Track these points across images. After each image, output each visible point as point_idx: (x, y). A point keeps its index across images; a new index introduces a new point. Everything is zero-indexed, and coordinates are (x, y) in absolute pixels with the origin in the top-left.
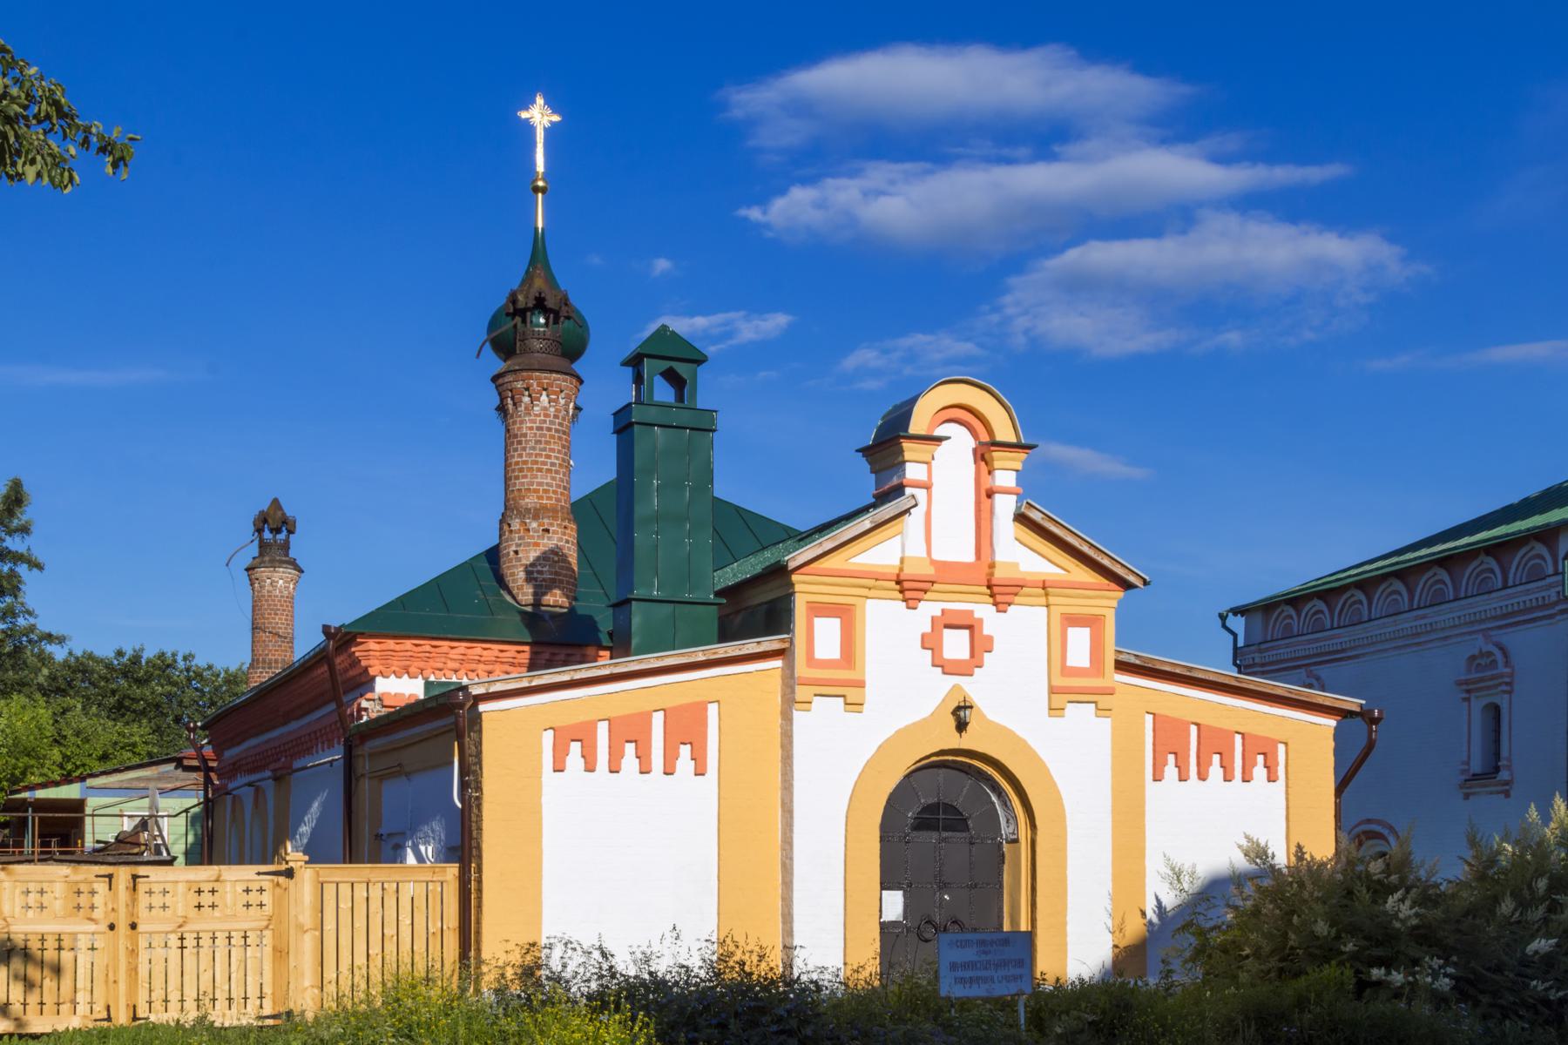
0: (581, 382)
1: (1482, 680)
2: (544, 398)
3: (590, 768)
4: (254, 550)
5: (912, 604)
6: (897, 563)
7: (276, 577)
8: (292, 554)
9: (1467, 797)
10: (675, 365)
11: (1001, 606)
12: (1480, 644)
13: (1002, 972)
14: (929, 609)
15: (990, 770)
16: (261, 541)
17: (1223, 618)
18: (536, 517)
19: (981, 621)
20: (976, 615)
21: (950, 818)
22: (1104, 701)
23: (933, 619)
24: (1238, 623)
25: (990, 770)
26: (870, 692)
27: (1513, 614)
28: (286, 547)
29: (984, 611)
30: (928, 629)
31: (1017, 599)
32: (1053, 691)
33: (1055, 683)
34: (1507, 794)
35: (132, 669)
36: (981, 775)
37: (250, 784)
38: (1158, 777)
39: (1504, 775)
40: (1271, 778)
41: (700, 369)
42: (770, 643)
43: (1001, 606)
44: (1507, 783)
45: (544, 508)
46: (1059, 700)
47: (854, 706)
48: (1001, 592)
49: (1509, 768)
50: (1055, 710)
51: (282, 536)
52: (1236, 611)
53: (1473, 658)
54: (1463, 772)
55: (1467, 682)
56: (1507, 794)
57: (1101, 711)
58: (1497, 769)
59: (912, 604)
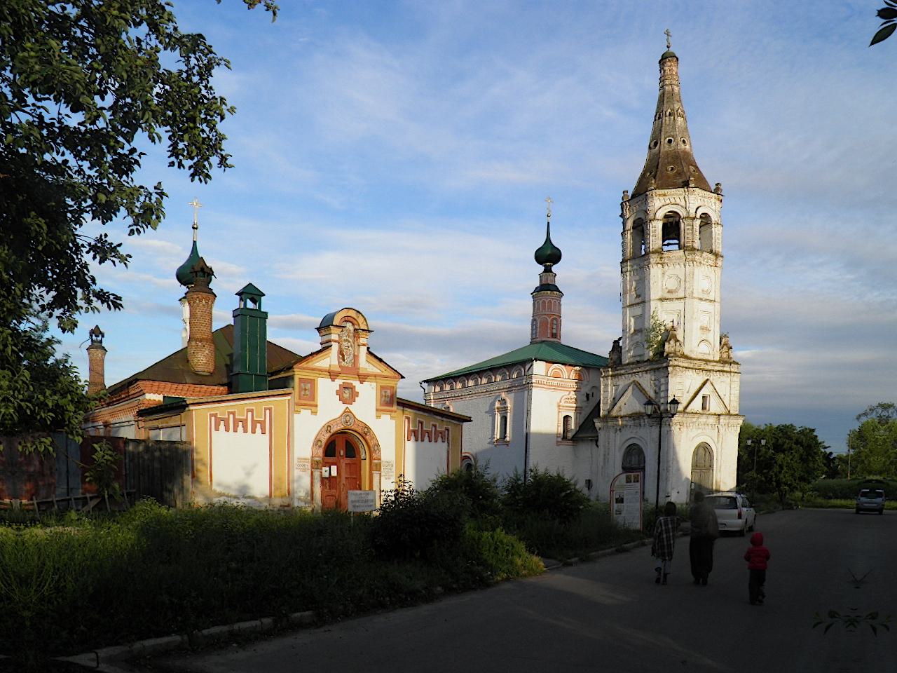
0: (216, 297)
2: (204, 302)
3: (245, 431)
4: (89, 343)
6: (328, 366)
7: (98, 352)
8: (103, 345)
14: (339, 382)
15: (356, 434)
16: (92, 340)
18: (200, 342)
19: (355, 387)
20: (354, 384)
21: (344, 446)
22: (393, 414)
23: (340, 385)
24: (425, 385)
25: (356, 434)
28: (101, 342)
29: (356, 383)
31: (367, 380)
32: (377, 410)
36: (345, 433)
37: (94, 427)
38: (217, 429)
40: (263, 433)
41: (262, 298)
45: (204, 338)
47: (314, 413)
48: (363, 378)
50: (378, 417)
51: (99, 338)
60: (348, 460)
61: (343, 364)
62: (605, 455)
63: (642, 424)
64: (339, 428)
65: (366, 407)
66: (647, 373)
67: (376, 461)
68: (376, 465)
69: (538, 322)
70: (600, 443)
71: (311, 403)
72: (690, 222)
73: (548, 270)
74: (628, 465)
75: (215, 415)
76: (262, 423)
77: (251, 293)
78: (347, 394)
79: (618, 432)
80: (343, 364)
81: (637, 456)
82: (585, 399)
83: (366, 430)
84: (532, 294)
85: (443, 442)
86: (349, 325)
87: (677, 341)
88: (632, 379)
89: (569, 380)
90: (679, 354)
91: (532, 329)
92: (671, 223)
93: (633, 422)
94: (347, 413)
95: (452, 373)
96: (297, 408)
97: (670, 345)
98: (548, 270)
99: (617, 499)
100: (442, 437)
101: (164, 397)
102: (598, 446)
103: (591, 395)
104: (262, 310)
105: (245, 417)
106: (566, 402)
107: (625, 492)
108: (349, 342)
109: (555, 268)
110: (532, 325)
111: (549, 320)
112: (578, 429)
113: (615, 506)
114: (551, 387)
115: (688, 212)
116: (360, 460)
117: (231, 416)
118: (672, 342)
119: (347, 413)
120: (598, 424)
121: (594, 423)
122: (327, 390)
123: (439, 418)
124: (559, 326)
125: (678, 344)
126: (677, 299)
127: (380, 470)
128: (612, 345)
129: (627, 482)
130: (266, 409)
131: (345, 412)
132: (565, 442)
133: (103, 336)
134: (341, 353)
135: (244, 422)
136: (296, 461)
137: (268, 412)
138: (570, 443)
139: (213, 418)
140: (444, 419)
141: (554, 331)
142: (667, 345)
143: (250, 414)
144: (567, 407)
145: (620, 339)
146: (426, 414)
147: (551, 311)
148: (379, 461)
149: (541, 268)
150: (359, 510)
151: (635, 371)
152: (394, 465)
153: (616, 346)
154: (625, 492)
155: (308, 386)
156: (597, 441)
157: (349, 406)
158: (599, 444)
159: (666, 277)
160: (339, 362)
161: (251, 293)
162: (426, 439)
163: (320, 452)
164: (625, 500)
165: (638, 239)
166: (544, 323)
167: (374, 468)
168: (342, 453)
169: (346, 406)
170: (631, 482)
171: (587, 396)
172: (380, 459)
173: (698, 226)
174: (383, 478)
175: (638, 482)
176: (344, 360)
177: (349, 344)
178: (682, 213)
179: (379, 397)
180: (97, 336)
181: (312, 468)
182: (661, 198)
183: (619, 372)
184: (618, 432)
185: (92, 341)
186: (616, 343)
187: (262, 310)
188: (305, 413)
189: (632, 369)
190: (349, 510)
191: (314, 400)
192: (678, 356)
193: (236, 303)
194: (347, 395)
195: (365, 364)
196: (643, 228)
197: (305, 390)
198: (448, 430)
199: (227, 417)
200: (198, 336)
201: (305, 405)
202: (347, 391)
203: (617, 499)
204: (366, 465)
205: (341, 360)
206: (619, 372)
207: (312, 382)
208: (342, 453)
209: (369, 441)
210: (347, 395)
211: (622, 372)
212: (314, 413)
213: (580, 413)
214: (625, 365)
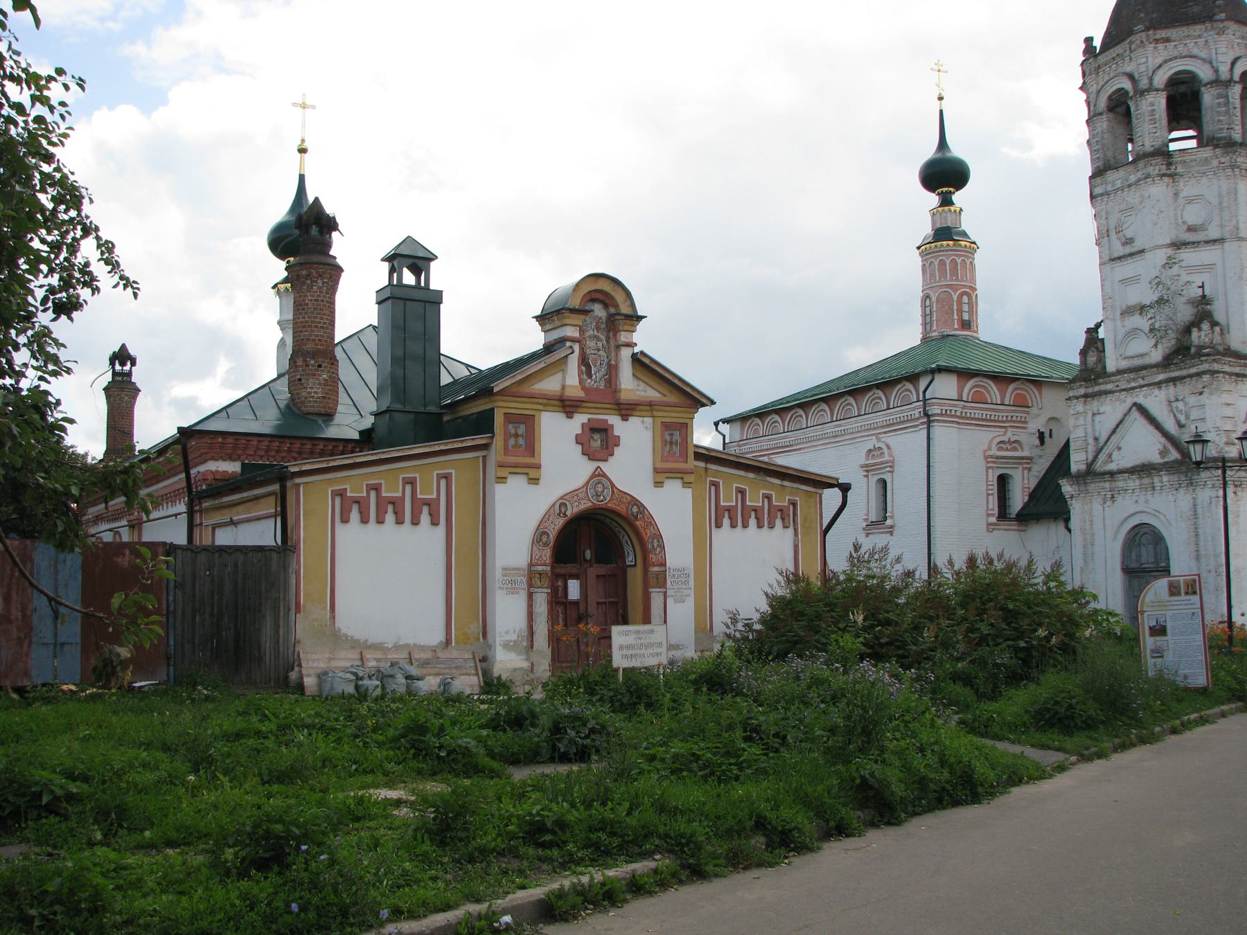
1: (875, 464)
5: (570, 415)
9: (867, 535)
10: (417, 262)
11: (625, 418)
12: (871, 443)
13: (650, 651)
14: (581, 419)
17: (716, 424)
18: (313, 358)
22: (688, 478)
24: (724, 428)
26: (545, 473)
27: (893, 424)
28: (130, 374)
29: (614, 420)
30: (580, 432)
32: (656, 471)
33: (658, 466)
34: (891, 533)
35: (1133, 467)
37: (110, 530)
38: (719, 525)
39: (889, 522)
40: (435, 523)
42: (479, 440)
43: (625, 418)
44: (892, 527)
46: (660, 478)
47: (534, 481)
48: (626, 410)
49: (892, 517)
50: (658, 484)
51: (127, 368)
52: (725, 421)
53: (870, 451)
54: (866, 520)
55: (866, 466)
56: (891, 533)
57: (686, 484)
58: (885, 519)
59: (570, 415)
60: (602, 569)
61: (589, 383)
62: (1085, 547)
63: (1158, 484)
64: (582, 507)
65: (632, 465)
66: (1160, 388)
67: (656, 569)
68: (657, 574)
69: (934, 299)
70: (1074, 522)
71: (528, 460)
72: (1221, 91)
73: (946, 201)
74: (1134, 565)
75: (341, 494)
76: (432, 505)
77: (411, 256)
78: (596, 443)
79: (1109, 503)
80: (589, 383)
81: (1151, 547)
82: (1037, 442)
83: (635, 509)
84: (918, 248)
85: (785, 527)
86: (599, 311)
87: (1214, 324)
88: (1130, 401)
89: (1002, 407)
90: (1221, 348)
91: (924, 316)
92: (1184, 95)
93: (1137, 482)
94: (598, 475)
95: (773, 404)
96: (503, 472)
97: (1203, 333)
98: (946, 201)
99: (1151, 628)
100: (783, 519)
101: (243, 465)
102: (1069, 530)
103: (1047, 435)
104: (432, 287)
105: (399, 494)
106: (1000, 449)
107: (1169, 613)
108: (598, 339)
109: (958, 197)
110: (924, 307)
111: (955, 298)
112: (1026, 498)
113: (1149, 642)
114: (963, 421)
115: (1216, 71)
116: (624, 569)
117: (373, 494)
118: (1205, 326)
119: (598, 475)
120: (1067, 488)
121: (1059, 487)
122: (558, 435)
123: (777, 481)
124: (972, 306)
125: (1217, 329)
126: (1207, 242)
127: (664, 585)
128: (1084, 336)
129: (1172, 594)
130: (440, 477)
131: (593, 476)
132: (1004, 525)
133: (133, 363)
134: (584, 360)
135: (396, 504)
136: (498, 574)
137: (443, 482)
138: (1014, 525)
139: (338, 500)
140: (786, 483)
141: (966, 317)
142: (1195, 333)
143: (408, 488)
144: (1003, 458)
145: (1098, 325)
146: (751, 475)
147: (957, 280)
148: (662, 569)
149: (933, 199)
150: (635, 663)
151: (1133, 384)
152: (692, 576)
153: (1093, 341)
154: (1169, 613)
155: (522, 429)
156: (1067, 520)
157: (601, 464)
158: (1072, 525)
159: (1180, 200)
160: (581, 381)
161: (411, 256)
162: (753, 522)
163: (547, 554)
164: (1169, 631)
165: (1120, 130)
166: (945, 301)
167: (652, 581)
168: (588, 554)
169: (595, 464)
170: (1179, 594)
171: (1041, 436)
172: (665, 565)
173: (1237, 96)
174: (669, 601)
175: (1195, 593)
176: (590, 376)
177: (600, 344)
178: (1204, 73)
179: (659, 445)
180: (123, 364)
181: (530, 585)
182: (1161, 46)
183: (1097, 389)
184: (1109, 503)
185: (115, 374)
186: (1092, 332)
187: (432, 287)
188: (516, 483)
189: (1129, 382)
190: (615, 665)
191: (533, 455)
192: (1219, 353)
193: (380, 276)
194: (598, 442)
195: (629, 384)
196: (1128, 109)
197: (516, 435)
198: (794, 504)
199: (365, 494)
200: (309, 347)
201: (516, 466)
202: (597, 436)
203: (1151, 628)
204: (635, 578)
205: (585, 377)
206: (1103, 387)
207: (529, 422)
208: (588, 554)
209: (642, 530)
210: (598, 442)
211: (1109, 387)
212: (534, 481)
213: (1029, 469)
214: (1113, 374)
